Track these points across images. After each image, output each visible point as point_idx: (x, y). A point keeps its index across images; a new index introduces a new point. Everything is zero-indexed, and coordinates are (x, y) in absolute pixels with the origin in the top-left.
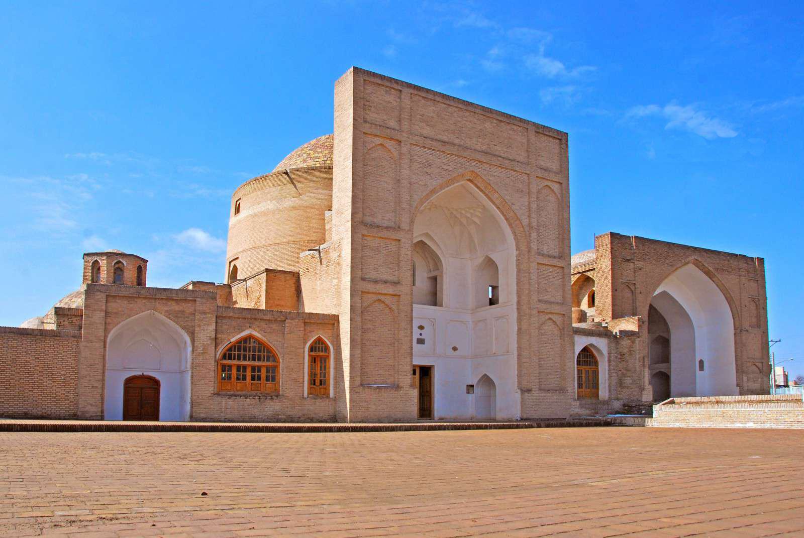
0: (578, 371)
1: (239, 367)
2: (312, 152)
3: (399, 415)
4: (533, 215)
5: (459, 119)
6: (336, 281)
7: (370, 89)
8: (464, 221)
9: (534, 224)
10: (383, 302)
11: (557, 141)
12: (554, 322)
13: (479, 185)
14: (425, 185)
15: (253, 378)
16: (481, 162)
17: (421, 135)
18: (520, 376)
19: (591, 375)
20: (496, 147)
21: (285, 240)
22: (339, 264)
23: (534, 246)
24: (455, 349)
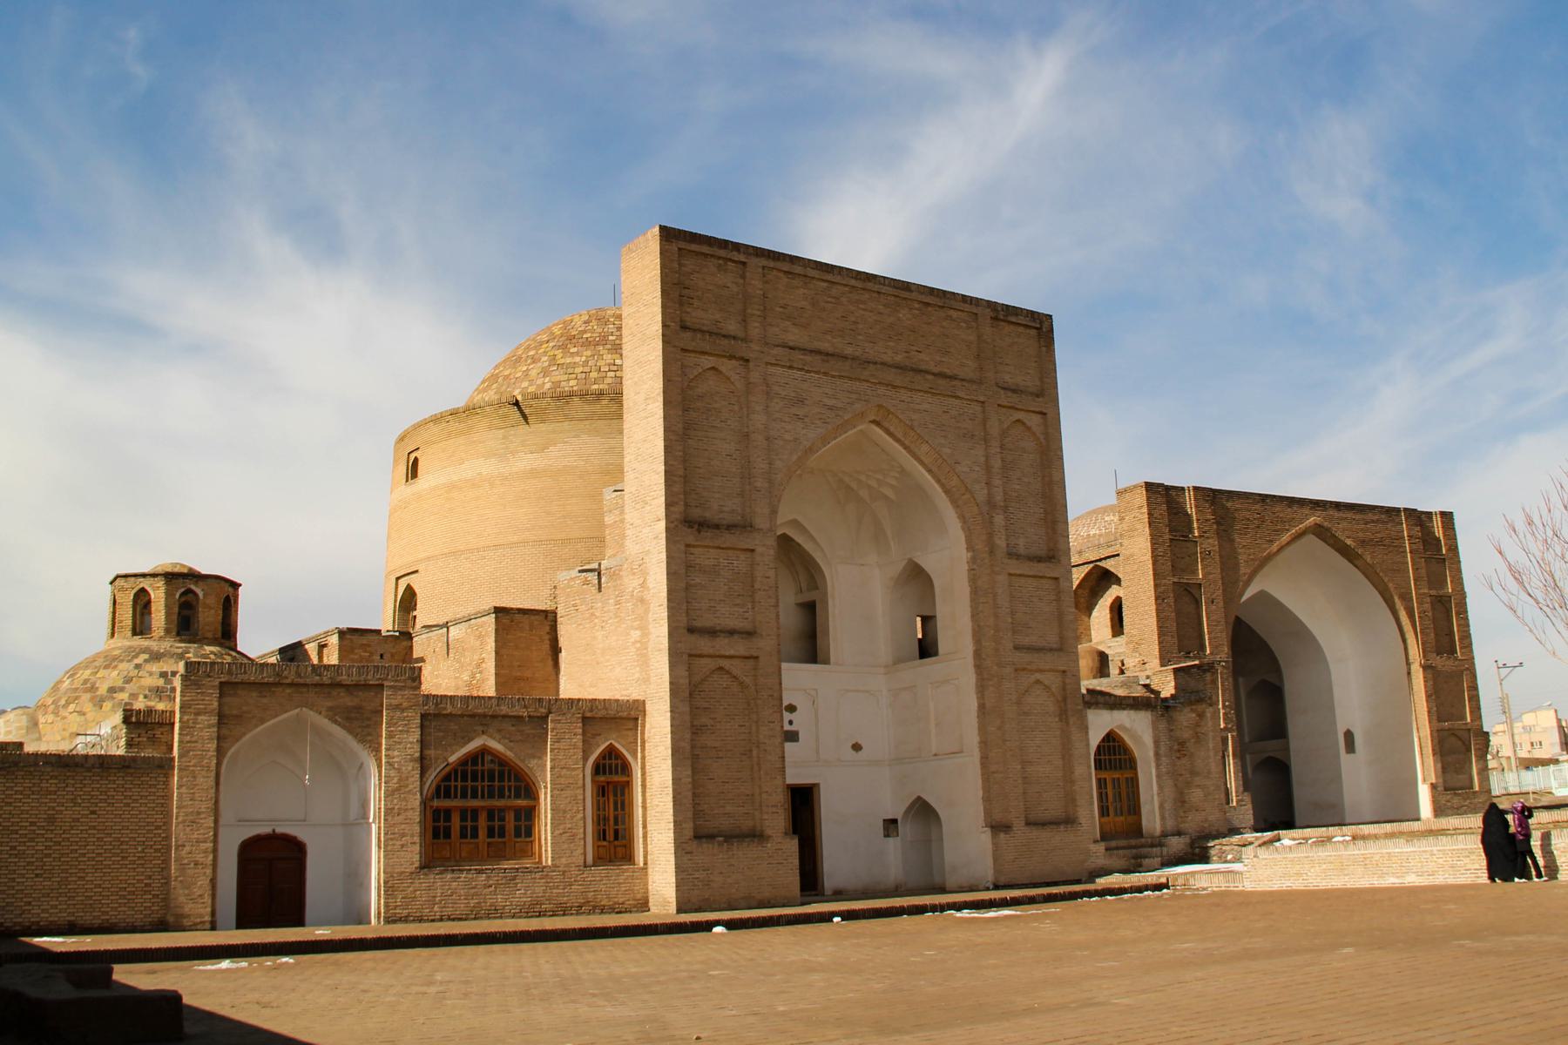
0: (1099, 781)
1: (464, 813)
2: (559, 353)
3: (766, 893)
4: (997, 482)
5: (852, 308)
6: (638, 633)
7: (690, 264)
8: (864, 493)
9: (999, 498)
10: (728, 672)
11: (1033, 332)
12: (1047, 688)
13: (892, 429)
14: (796, 440)
15: (491, 833)
16: (895, 387)
17: (785, 346)
18: (987, 799)
19: (1123, 786)
20: (922, 356)
21: (515, 539)
22: (642, 601)
23: (1001, 542)
24: (857, 747)
